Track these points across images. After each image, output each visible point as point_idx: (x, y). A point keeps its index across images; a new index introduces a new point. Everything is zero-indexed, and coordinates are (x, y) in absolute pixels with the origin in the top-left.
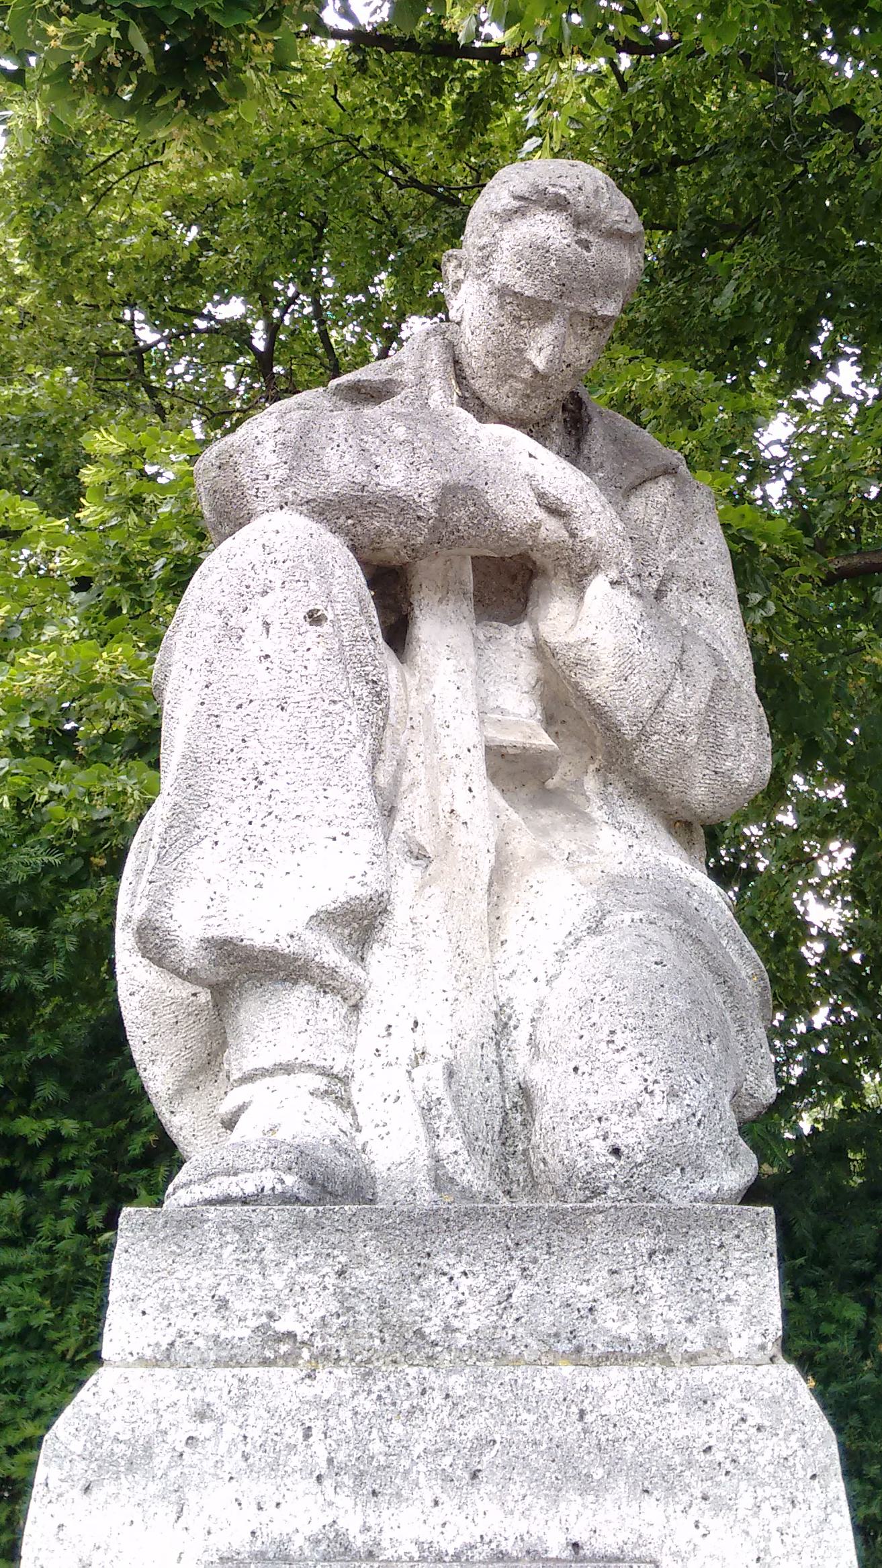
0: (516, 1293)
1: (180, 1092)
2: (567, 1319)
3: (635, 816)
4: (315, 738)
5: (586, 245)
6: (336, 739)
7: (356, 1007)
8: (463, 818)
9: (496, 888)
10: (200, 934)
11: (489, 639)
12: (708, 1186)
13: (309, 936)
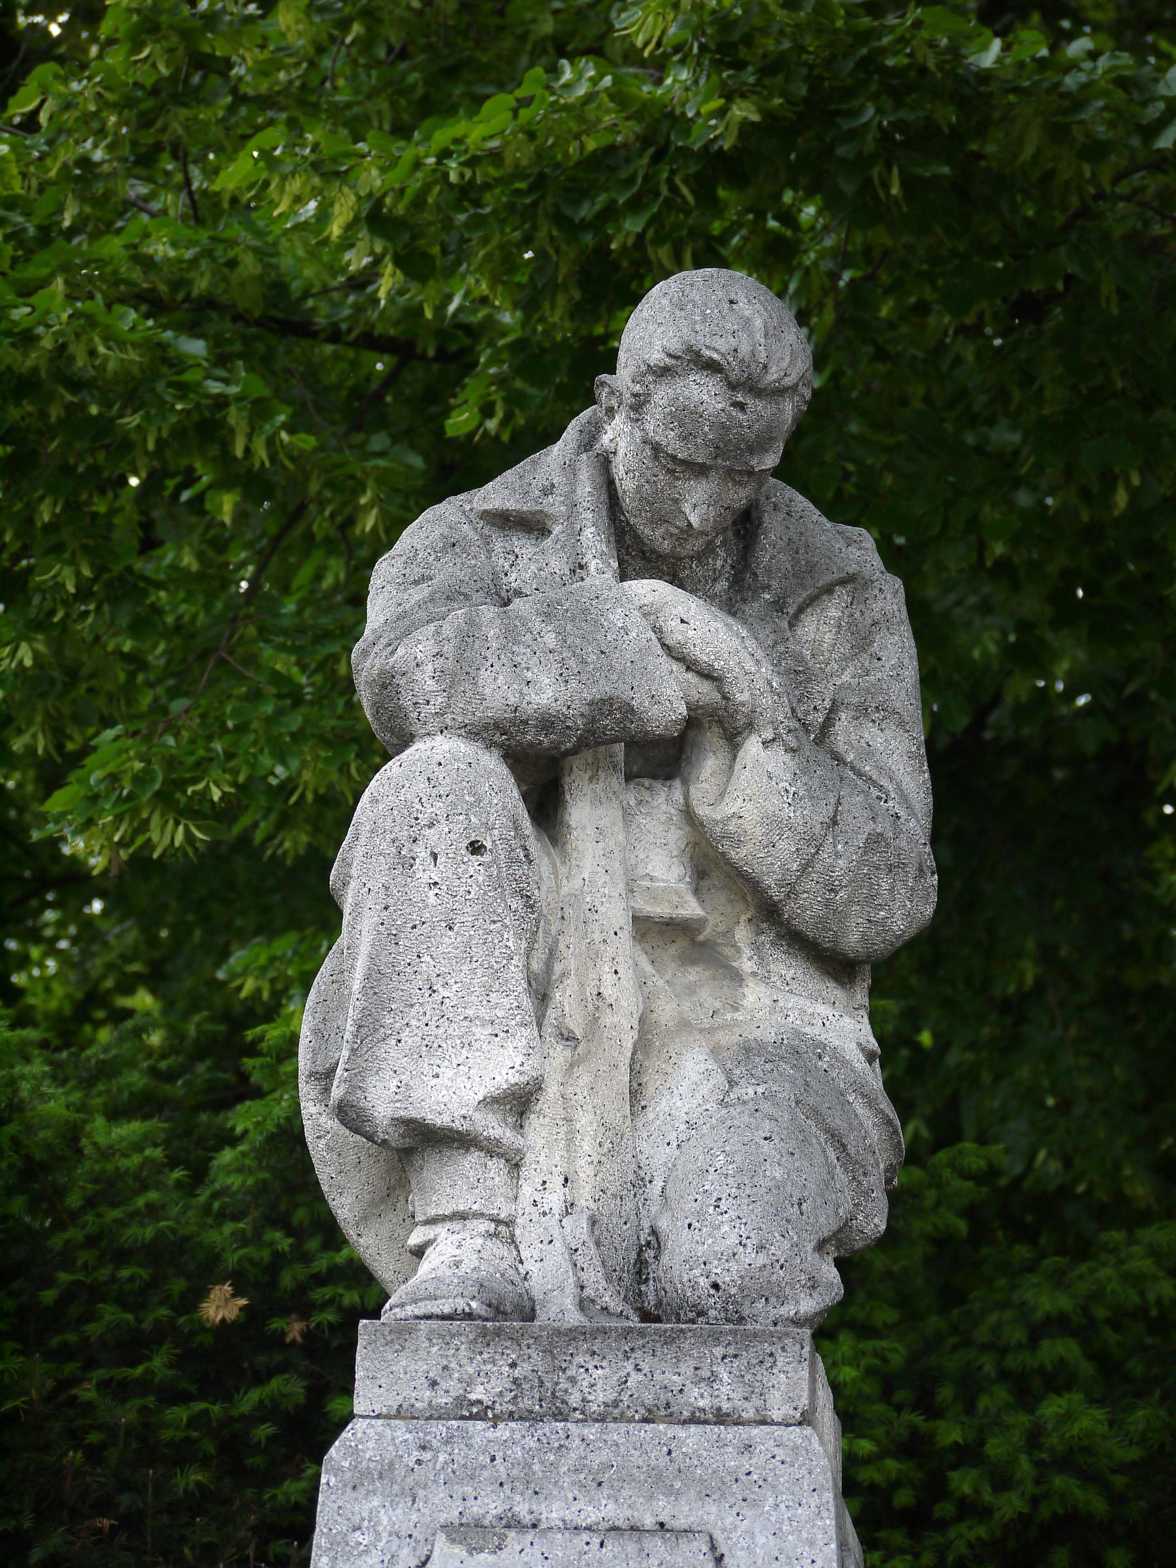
0: (630, 1380)
1: (365, 1218)
2: (664, 1397)
3: (787, 967)
4: (478, 952)
5: (741, 406)
6: (497, 953)
7: (517, 1166)
8: (609, 1001)
9: (639, 1056)
10: (389, 1113)
11: (640, 803)
12: (788, 1310)
13: (477, 1116)
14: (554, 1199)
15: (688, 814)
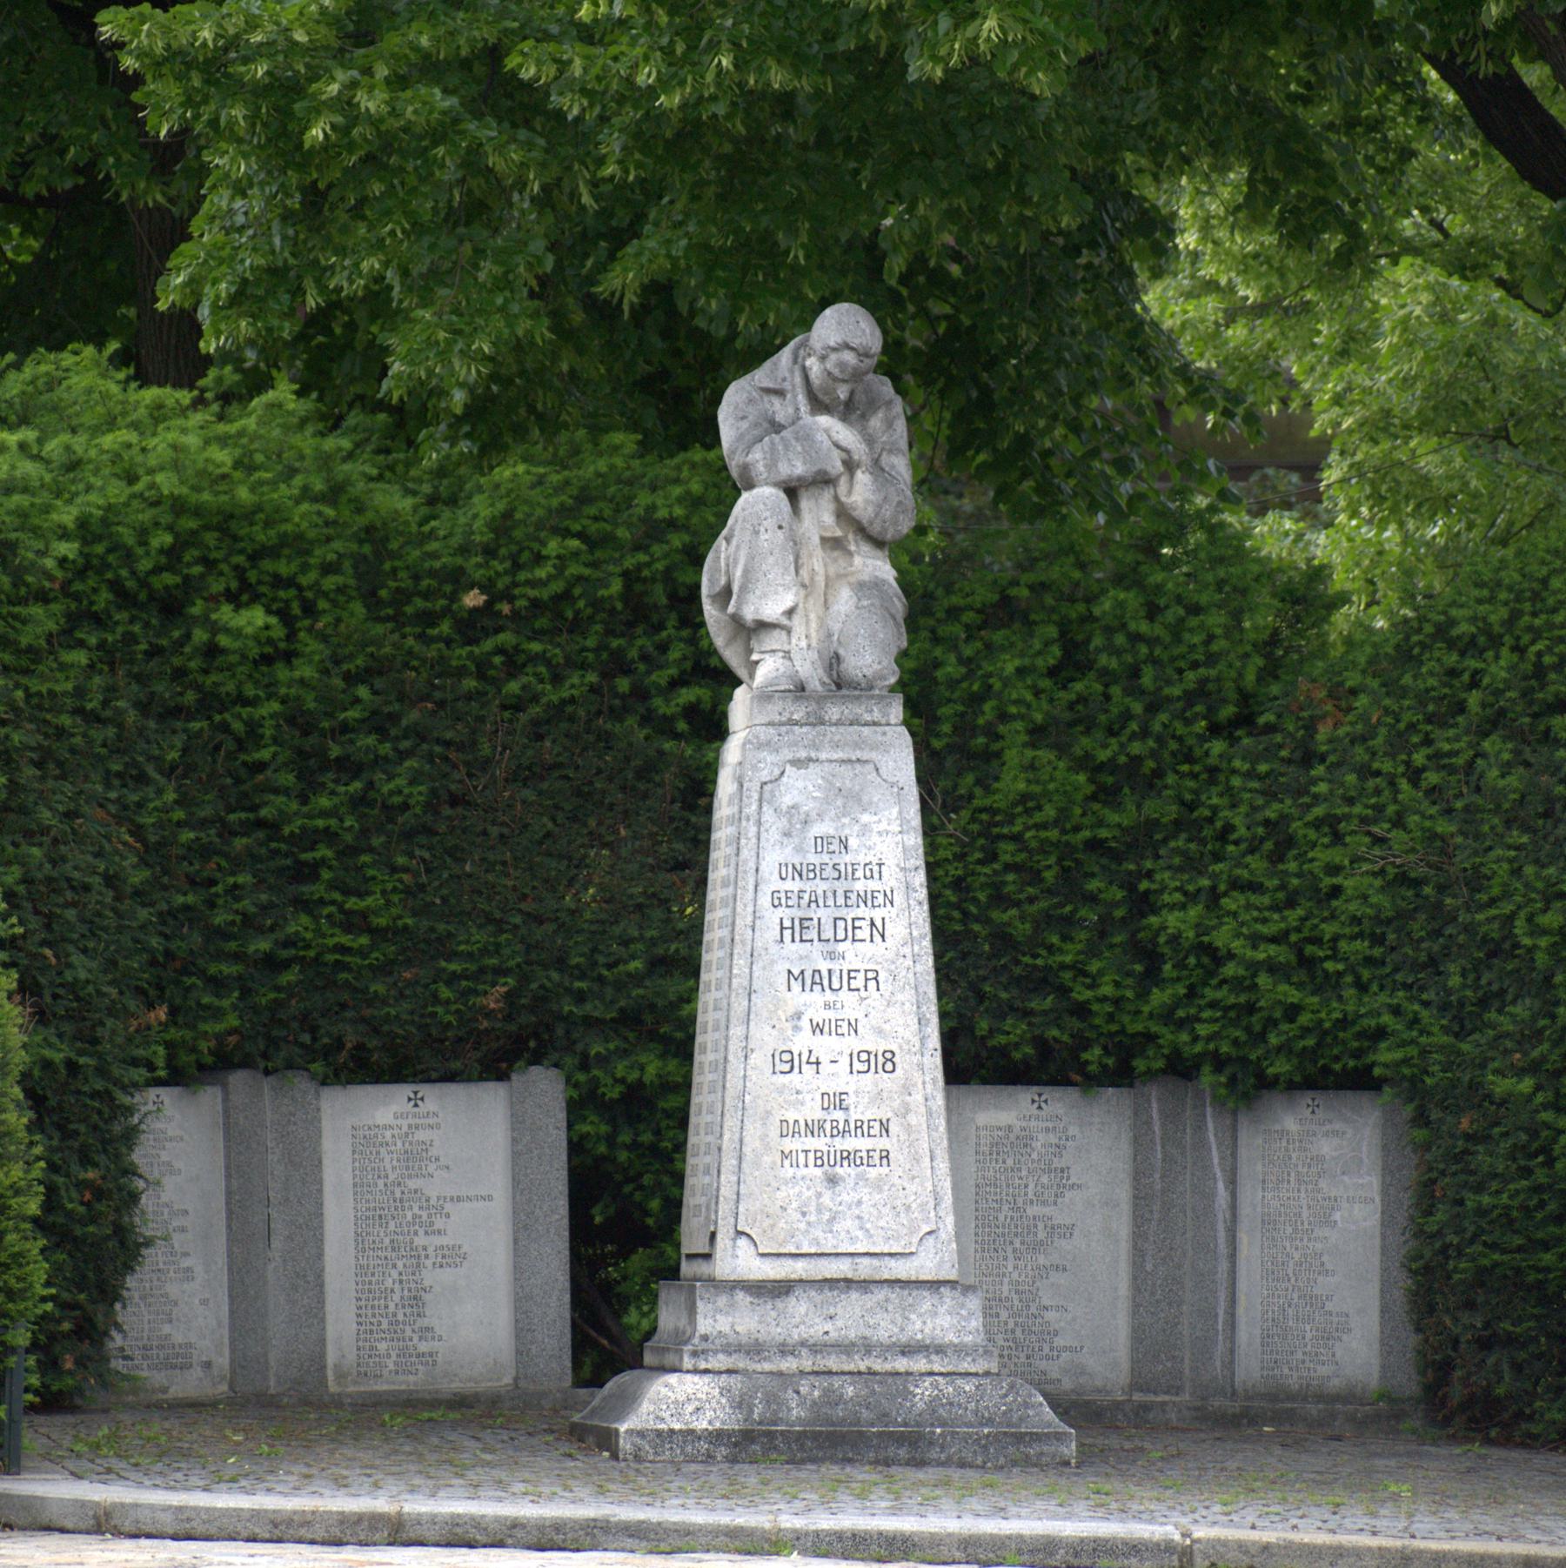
3: (866, 548)
14: (803, 644)
15: (836, 499)
